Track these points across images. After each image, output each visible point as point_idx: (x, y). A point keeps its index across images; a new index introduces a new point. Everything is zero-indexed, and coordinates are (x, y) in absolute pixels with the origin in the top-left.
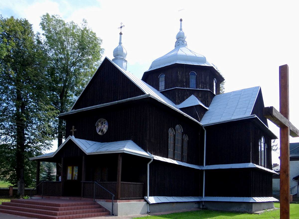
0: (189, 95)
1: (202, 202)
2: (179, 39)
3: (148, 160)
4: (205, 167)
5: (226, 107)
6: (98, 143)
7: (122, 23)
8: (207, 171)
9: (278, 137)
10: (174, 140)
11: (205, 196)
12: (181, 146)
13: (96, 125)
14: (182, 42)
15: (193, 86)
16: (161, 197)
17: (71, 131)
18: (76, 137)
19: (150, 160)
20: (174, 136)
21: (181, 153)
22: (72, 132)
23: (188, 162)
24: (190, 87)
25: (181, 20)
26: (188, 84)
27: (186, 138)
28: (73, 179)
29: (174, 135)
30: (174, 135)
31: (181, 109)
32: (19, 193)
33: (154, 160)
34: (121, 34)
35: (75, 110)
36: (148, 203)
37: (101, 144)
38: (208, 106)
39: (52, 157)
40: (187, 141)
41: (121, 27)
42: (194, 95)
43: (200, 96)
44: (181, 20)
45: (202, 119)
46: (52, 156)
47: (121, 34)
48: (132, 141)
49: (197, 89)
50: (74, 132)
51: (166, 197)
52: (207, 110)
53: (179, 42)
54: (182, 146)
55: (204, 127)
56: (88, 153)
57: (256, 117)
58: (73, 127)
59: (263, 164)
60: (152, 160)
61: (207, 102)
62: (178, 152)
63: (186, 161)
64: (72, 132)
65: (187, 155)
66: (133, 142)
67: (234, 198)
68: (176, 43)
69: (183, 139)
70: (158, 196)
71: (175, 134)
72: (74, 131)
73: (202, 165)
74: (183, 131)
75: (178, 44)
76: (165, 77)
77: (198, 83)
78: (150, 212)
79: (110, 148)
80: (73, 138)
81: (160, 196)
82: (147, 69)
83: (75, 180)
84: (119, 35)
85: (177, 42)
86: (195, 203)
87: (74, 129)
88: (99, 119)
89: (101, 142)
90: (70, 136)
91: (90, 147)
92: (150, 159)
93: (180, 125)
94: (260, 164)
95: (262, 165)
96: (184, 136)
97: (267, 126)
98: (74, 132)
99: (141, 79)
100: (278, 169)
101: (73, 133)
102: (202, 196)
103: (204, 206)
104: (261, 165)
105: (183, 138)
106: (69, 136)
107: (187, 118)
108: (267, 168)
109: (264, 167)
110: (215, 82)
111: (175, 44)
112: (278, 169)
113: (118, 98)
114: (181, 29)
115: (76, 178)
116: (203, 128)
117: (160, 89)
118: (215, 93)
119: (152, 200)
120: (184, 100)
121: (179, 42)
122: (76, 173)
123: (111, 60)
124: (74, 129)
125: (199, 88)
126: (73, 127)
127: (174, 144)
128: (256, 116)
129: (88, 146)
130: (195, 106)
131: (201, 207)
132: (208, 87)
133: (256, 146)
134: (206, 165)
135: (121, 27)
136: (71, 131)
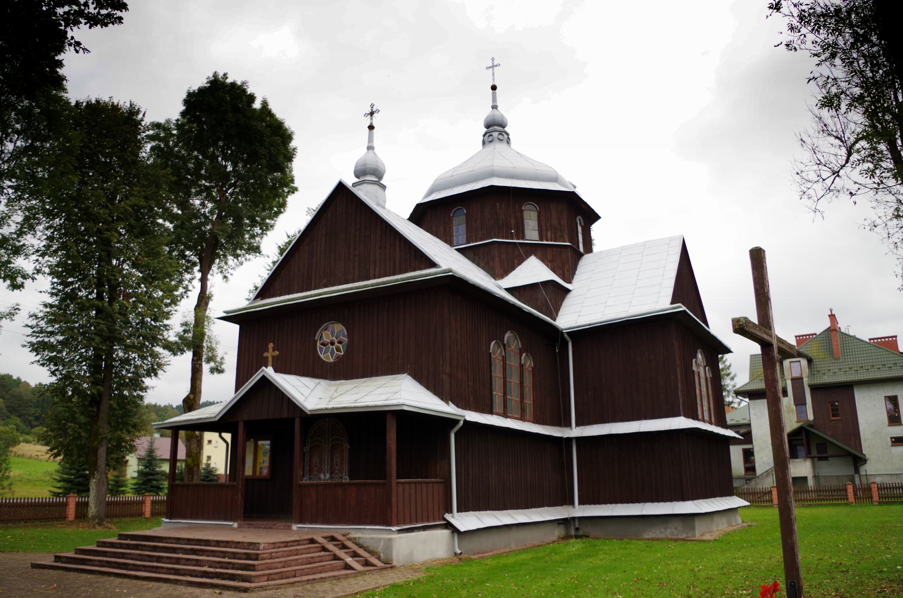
0: (751, 463)
1: (574, 519)
2: (490, 129)
3: (450, 422)
4: (576, 432)
5: (612, 285)
6: (324, 383)
7: (372, 106)
8: (580, 440)
9: (731, 350)
10: (504, 369)
11: (581, 503)
12: (518, 382)
13: (316, 339)
14: (499, 134)
15: (532, 235)
16: (482, 512)
17: (265, 355)
18: (276, 371)
19: (457, 422)
20: (504, 359)
21: (519, 400)
22: (267, 358)
23: (537, 421)
24: (527, 238)
25: (494, 88)
26: (521, 234)
27: (529, 364)
28: (258, 474)
29: (503, 356)
30: (503, 356)
31: (509, 290)
32: (92, 513)
33: (465, 421)
34: (371, 127)
35: (262, 299)
36: (455, 530)
37: (331, 385)
38: (570, 282)
39: (214, 420)
40: (531, 369)
41: (372, 114)
42: (535, 256)
43: (549, 257)
44: (494, 88)
45: (559, 314)
46: (215, 417)
47: (371, 127)
48: (409, 377)
49: (542, 241)
50: (273, 357)
51: (494, 512)
52: (568, 291)
53: (492, 135)
54: (521, 383)
55: (567, 333)
56: (310, 411)
57: (685, 311)
58: (271, 345)
59: (706, 418)
60: (462, 422)
61: (567, 271)
62: (514, 397)
63: (532, 419)
64: (267, 358)
65: (532, 403)
66: (411, 378)
67: (649, 505)
68: (484, 136)
69: (522, 366)
70: (476, 511)
71: (504, 354)
72: (268, 352)
73: (568, 424)
74: (520, 346)
75: (491, 138)
76: (467, 214)
77: (544, 228)
78: (461, 553)
79: (360, 395)
80: (269, 371)
81: (479, 510)
82: (420, 199)
83: (261, 480)
84: (368, 129)
85: (487, 135)
86: (559, 524)
87: (274, 351)
88: (325, 323)
89: (330, 380)
90: (264, 368)
91: (310, 394)
92: (457, 421)
93: (515, 333)
94: (700, 417)
95: (705, 418)
96: (523, 357)
97: (709, 328)
98: (273, 357)
99: (408, 216)
100: (733, 420)
101: (270, 359)
102: (572, 503)
103: (580, 531)
104: (704, 421)
105: (523, 362)
106: (261, 367)
107: (530, 315)
108: (715, 425)
109: (711, 423)
110: (581, 225)
111: (482, 138)
112: (733, 420)
113: (372, 274)
114: (494, 107)
115: (265, 472)
116: (566, 335)
117: (455, 242)
118: (581, 249)
119: (466, 521)
120: (513, 268)
121: (493, 134)
122: (264, 461)
123: (351, 185)
124: (274, 351)
125: (547, 241)
126: (271, 345)
127: (505, 378)
128: (684, 308)
129: (306, 392)
130: (542, 283)
131: (573, 532)
132: (566, 237)
133: (689, 376)
134: (577, 425)
135: (372, 114)
136: (265, 355)
